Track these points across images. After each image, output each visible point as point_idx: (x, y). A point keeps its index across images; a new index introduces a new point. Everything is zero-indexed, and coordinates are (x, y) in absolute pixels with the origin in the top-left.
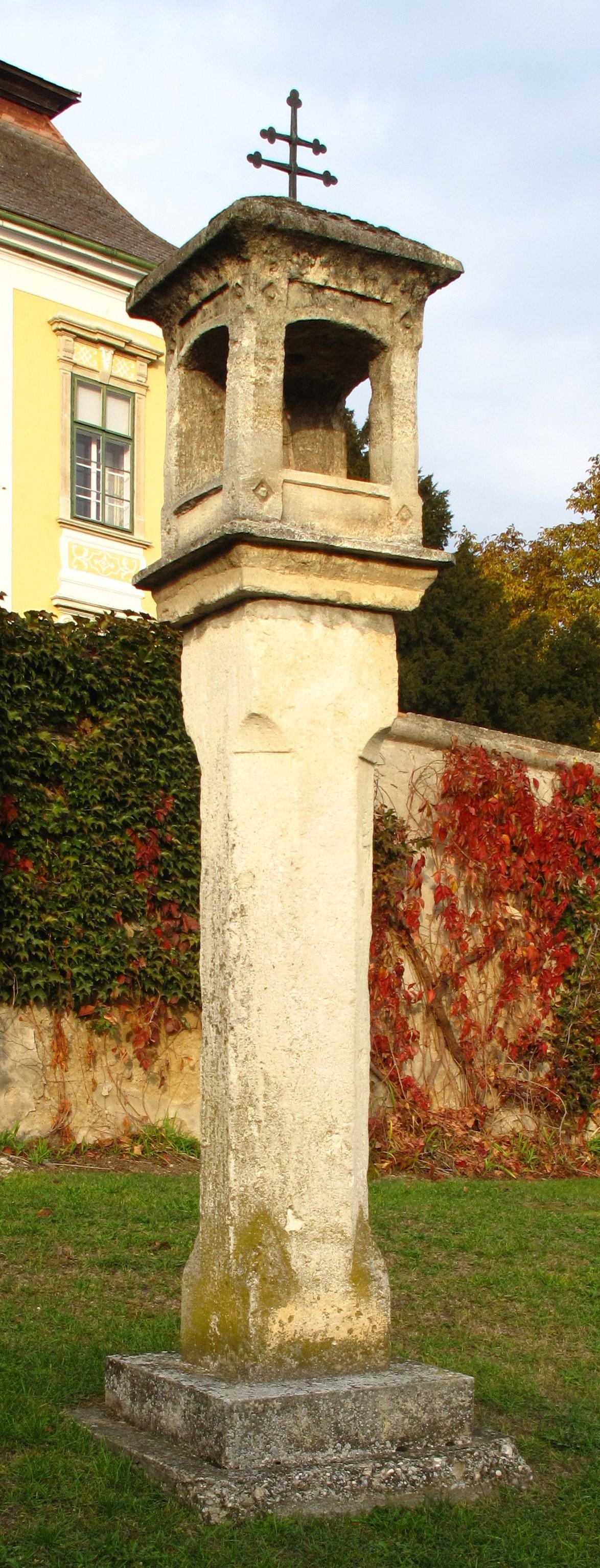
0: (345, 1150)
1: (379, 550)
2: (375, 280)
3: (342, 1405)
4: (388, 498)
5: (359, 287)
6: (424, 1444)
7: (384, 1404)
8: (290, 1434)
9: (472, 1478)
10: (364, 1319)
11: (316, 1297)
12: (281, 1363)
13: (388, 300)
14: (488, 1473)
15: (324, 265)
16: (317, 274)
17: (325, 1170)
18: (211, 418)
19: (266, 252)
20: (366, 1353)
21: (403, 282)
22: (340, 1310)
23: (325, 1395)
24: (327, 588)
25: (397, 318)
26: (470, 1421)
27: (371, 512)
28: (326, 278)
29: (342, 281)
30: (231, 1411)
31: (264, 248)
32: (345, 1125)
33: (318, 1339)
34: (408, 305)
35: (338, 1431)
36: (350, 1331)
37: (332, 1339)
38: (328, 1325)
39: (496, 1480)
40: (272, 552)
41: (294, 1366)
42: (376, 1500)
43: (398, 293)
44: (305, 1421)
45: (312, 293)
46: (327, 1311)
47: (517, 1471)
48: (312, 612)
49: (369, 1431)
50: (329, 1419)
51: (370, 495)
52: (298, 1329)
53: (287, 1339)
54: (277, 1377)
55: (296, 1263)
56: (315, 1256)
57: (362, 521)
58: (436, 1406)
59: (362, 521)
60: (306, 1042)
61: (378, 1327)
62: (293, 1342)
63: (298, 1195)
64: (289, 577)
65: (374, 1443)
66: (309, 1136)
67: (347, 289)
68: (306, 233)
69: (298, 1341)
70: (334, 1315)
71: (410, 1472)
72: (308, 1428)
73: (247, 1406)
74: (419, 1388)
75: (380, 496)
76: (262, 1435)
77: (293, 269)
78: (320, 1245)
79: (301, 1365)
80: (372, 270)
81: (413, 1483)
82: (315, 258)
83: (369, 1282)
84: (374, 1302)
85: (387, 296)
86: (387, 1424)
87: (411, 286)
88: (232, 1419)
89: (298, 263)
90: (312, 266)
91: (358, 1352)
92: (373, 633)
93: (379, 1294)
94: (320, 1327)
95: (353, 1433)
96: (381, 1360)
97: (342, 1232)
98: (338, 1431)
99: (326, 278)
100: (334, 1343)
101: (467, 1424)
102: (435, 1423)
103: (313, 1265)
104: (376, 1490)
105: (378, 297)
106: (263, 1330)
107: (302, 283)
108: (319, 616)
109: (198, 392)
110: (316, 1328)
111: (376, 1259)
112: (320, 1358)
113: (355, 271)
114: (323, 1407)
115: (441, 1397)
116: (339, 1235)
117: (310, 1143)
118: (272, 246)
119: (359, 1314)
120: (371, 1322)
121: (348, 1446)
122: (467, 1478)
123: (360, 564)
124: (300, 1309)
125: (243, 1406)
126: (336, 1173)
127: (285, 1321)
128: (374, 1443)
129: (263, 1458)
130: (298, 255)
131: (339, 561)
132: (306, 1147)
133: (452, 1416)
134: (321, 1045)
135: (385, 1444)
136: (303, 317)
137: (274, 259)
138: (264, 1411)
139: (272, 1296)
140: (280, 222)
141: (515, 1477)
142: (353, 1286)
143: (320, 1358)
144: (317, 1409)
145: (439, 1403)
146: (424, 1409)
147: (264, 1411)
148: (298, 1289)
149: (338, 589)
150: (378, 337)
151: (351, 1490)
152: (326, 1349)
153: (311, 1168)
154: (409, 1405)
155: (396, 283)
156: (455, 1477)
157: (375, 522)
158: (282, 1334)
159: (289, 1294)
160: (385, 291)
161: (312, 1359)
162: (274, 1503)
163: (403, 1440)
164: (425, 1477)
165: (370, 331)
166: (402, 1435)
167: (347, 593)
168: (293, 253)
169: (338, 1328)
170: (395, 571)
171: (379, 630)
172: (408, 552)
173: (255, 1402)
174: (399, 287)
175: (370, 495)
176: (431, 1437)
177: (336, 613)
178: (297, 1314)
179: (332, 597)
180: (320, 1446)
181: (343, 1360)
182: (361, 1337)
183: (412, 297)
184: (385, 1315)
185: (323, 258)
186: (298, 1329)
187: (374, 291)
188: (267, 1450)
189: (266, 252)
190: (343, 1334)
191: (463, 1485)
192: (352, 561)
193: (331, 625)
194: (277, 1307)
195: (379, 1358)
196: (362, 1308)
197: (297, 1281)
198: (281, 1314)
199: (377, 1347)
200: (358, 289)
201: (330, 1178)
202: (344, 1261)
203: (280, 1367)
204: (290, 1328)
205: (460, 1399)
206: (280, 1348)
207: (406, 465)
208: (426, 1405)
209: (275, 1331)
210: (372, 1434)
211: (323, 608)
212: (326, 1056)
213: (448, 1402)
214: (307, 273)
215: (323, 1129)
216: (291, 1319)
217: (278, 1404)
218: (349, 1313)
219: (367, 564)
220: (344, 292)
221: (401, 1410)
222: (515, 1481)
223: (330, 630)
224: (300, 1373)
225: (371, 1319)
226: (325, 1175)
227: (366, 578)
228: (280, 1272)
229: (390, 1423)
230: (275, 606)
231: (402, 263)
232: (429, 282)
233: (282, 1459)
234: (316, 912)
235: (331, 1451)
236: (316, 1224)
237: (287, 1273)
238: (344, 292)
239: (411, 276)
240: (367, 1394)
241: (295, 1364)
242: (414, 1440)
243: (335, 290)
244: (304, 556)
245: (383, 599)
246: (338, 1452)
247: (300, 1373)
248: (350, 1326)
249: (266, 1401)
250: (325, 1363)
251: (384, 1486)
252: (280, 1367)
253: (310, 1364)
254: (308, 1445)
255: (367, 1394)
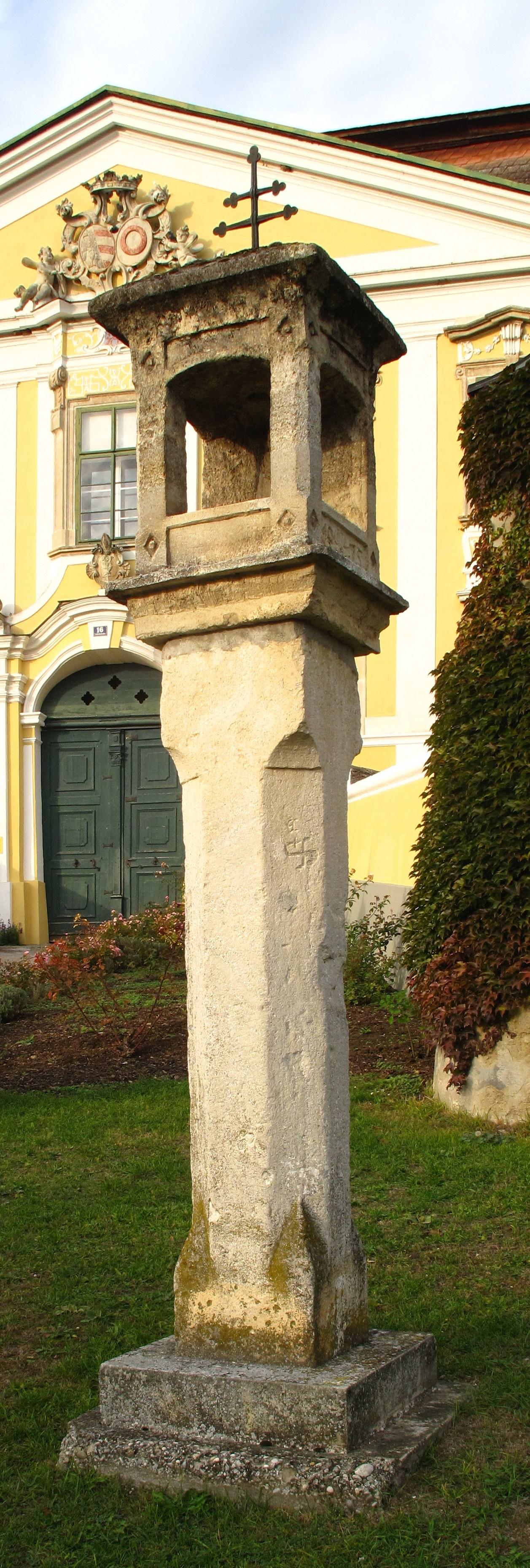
0: (259, 1149)
1: (235, 567)
2: (243, 303)
3: (205, 1389)
4: (268, 510)
5: (230, 317)
6: (292, 1443)
7: (247, 1397)
8: (156, 1406)
9: (298, 1487)
10: (282, 1313)
11: (233, 1286)
12: (201, 1342)
13: (263, 315)
14: (317, 1487)
15: (189, 314)
16: (187, 325)
17: (239, 1168)
18: (231, 476)
19: (136, 328)
20: (284, 1346)
21: (269, 292)
22: (257, 1302)
23: (188, 1376)
24: (214, 615)
25: (275, 328)
26: (342, 1432)
27: (255, 528)
28: (197, 324)
29: (213, 320)
30: (103, 1374)
31: (133, 325)
32: (259, 1125)
33: (236, 1325)
34: (285, 311)
35: (203, 1413)
36: (268, 1323)
37: (250, 1328)
38: (245, 1314)
39: (325, 1496)
40: (151, 598)
41: (213, 1347)
42: (194, 1483)
43: (271, 304)
44: (169, 1397)
45: (189, 343)
46: (245, 1301)
47: (353, 1493)
48: (210, 641)
49: (232, 1419)
50: (193, 1400)
51: (249, 513)
52: (217, 1314)
53: (206, 1321)
54: (198, 1353)
55: (215, 1253)
56: (232, 1247)
57: (246, 540)
58: (304, 1409)
59: (246, 540)
60: (217, 1046)
61: (297, 1323)
62: (213, 1325)
63: (214, 1189)
64: (177, 615)
65: (239, 1431)
66: (222, 1135)
67: (220, 325)
68: (152, 297)
69: (216, 1324)
70: (251, 1305)
71: (233, 1465)
72: (173, 1403)
73: (116, 1373)
74: (284, 1388)
75: (260, 510)
76: (130, 1400)
77: (164, 330)
78: (236, 1237)
79: (220, 1347)
80: (234, 297)
81: (233, 1476)
82: (179, 311)
83: (287, 1278)
84: (292, 1298)
85: (260, 312)
86: (251, 1416)
87: (279, 292)
88: (103, 1381)
89: (166, 324)
90: (180, 320)
91: (277, 1344)
92: (273, 644)
93: (298, 1291)
94: (238, 1314)
95: (217, 1418)
96: (301, 1356)
97: (258, 1228)
98: (203, 1413)
99: (197, 324)
100: (253, 1333)
101: (339, 1435)
102: (302, 1426)
103: (230, 1255)
104: (194, 1474)
105: (251, 318)
106: (184, 1309)
107: (178, 339)
108: (217, 643)
109: (220, 457)
110: (234, 1315)
111: (298, 1257)
112: (239, 1344)
113: (220, 305)
114: (187, 1388)
115: (309, 1401)
116: (255, 1230)
117: (224, 1142)
118: (137, 321)
119: (277, 1308)
120: (289, 1317)
121: (213, 1428)
122: (292, 1486)
123: (236, 583)
124: (217, 1295)
125: (113, 1373)
126: (250, 1171)
127: (204, 1304)
128: (239, 1431)
129: (133, 1422)
130: (164, 317)
131: (213, 587)
132: (220, 1145)
133: (321, 1422)
134: (233, 1049)
135: (250, 1435)
136: (180, 370)
137: (145, 330)
138: (131, 1380)
139: (191, 1280)
140: (128, 299)
141: (350, 1498)
142: (270, 1281)
143: (239, 1344)
144: (180, 1387)
145: (306, 1407)
146: (290, 1409)
147: (131, 1380)
148: (216, 1277)
149: (225, 613)
150: (257, 355)
151: (173, 1468)
152: (244, 1336)
153: (225, 1165)
154: (274, 1402)
155: (263, 296)
156: (282, 1481)
157: (259, 537)
158: (202, 1316)
159: (207, 1280)
160: (257, 309)
161: (231, 1343)
162: (98, 1461)
163: (268, 1435)
164: (245, 1473)
165: (248, 354)
166: (268, 1430)
167: (234, 614)
168: (159, 317)
169: (255, 1318)
170: (272, 579)
171: (281, 638)
172: (264, 559)
173: (124, 1370)
174: (269, 298)
175: (249, 513)
176: (299, 1438)
177: (234, 636)
178: (215, 1299)
179: (220, 621)
180: (185, 1422)
181: (260, 1349)
182: (280, 1331)
183: (286, 301)
184: (305, 1313)
185: (187, 309)
186: (217, 1314)
187: (245, 314)
188: (136, 1415)
189: (136, 328)
190: (260, 1324)
191: (286, 1491)
192: (227, 583)
193: (229, 647)
194: (196, 1291)
195: (300, 1354)
196: (279, 1302)
197: (215, 1269)
198: (201, 1297)
199: (296, 1342)
200: (230, 319)
201: (245, 1175)
202: (260, 1256)
203: (200, 1345)
204: (209, 1311)
205: (330, 1407)
206: (200, 1328)
207: (285, 470)
208: (292, 1406)
209: (195, 1312)
210: (237, 1421)
211: (221, 634)
212: (237, 1060)
213: (317, 1408)
214: (178, 328)
215: (236, 1128)
216: (209, 1303)
217: (144, 1376)
218: (266, 1306)
219: (242, 581)
220: (219, 329)
221: (266, 1406)
222: (349, 1502)
223: (229, 652)
224: (219, 1354)
225: (290, 1315)
226: (239, 1172)
227: (250, 594)
228: (201, 1259)
229: (254, 1417)
230: (176, 645)
231: (254, 277)
232: (293, 279)
233: (150, 1426)
234: (224, 923)
235: (195, 1429)
236: (231, 1217)
237: (207, 1260)
238: (219, 329)
239: (273, 284)
240: (229, 1384)
241: (214, 1345)
242: (280, 1438)
243: (211, 330)
244: (180, 593)
245: (269, 609)
246: (202, 1432)
247: (219, 1354)
248: (268, 1318)
249: (133, 1371)
250: (243, 1350)
251: (203, 1471)
252: (200, 1345)
253: (230, 1348)
254: (174, 1419)
255: (229, 1384)
